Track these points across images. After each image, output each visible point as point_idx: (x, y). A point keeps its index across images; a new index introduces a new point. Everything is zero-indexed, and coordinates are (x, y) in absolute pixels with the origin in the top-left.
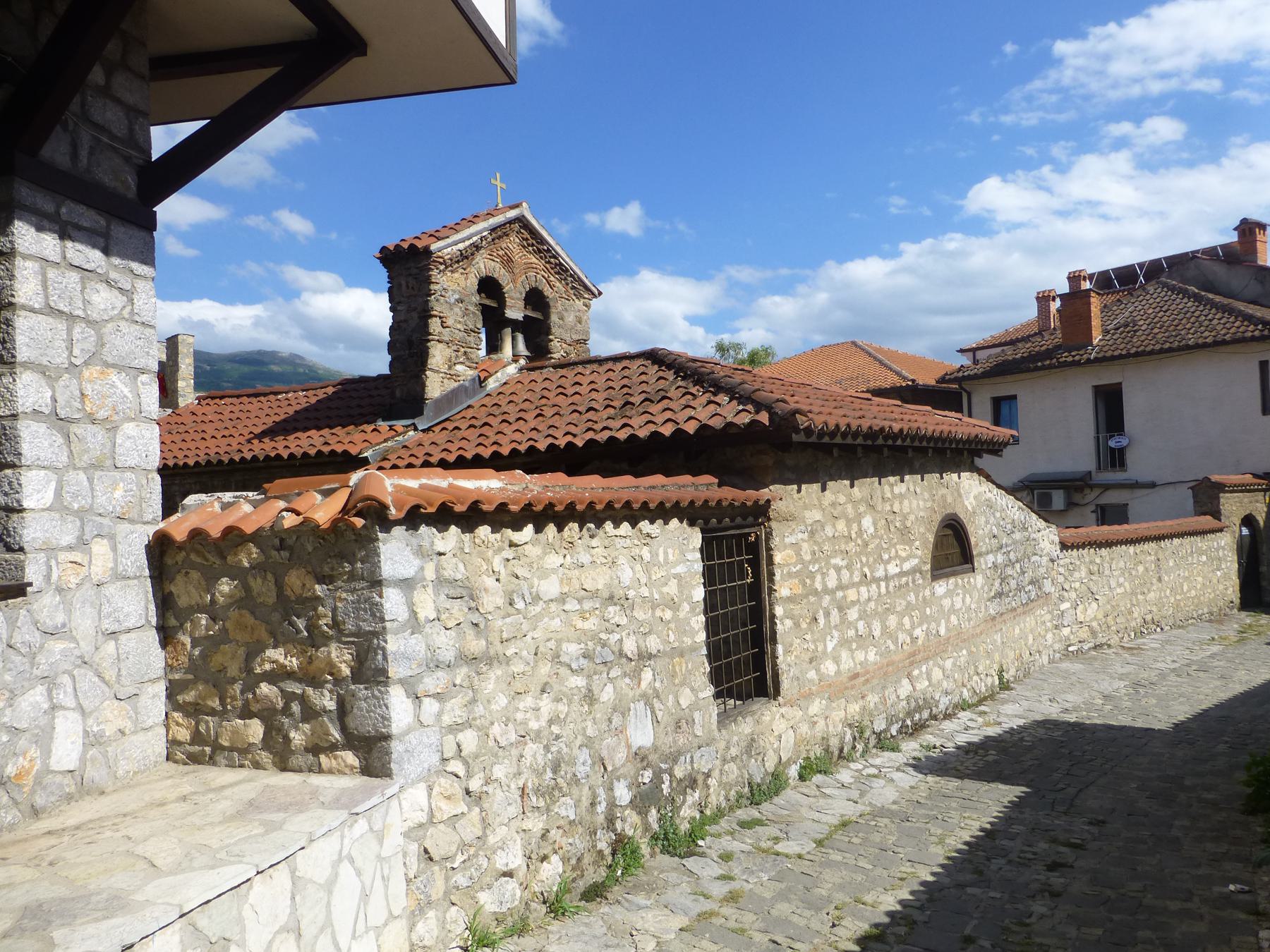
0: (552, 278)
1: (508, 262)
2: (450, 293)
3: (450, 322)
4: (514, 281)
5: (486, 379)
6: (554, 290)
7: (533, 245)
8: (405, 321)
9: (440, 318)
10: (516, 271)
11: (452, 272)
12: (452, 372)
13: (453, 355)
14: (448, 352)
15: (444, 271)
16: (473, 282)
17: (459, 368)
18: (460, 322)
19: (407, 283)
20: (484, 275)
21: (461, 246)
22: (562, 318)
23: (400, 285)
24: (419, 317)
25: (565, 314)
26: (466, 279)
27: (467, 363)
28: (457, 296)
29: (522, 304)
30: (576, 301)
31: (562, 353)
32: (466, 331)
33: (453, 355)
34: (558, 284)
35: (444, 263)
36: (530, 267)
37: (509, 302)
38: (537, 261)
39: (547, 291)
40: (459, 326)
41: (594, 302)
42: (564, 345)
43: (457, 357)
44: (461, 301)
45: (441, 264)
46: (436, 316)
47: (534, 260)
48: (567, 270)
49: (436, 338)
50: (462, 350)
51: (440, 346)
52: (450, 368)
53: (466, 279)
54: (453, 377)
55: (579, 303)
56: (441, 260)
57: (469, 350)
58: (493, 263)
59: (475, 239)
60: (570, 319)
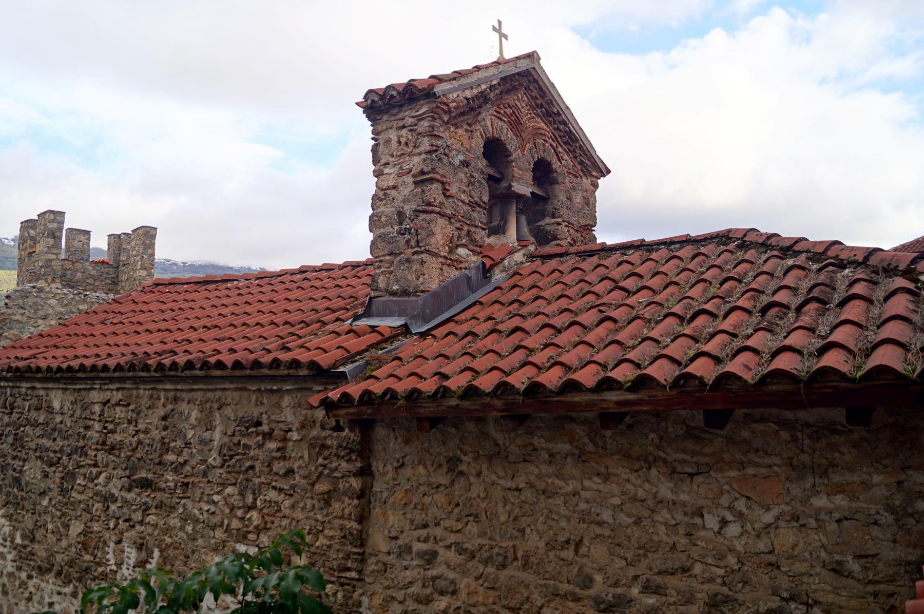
0: (560, 149)
1: (516, 124)
2: (454, 152)
3: (453, 190)
4: (522, 148)
5: (492, 267)
6: (562, 164)
7: (542, 106)
8: (394, 187)
9: (443, 183)
10: (524, 135)
11: (456, 126)
12: (453, 257)
13: (456, 233)
14: (450, 229)
15: (447, 123)
16: (478, 143)
17: (462, 251)
18: (464, 191)
19: (399, 137)
20: (490, 135)
21: (468, 94)
22: (569, 199)
23: (388, 141)
24: (416, 183)
25: (573, 194)
26: (470, 138)
27: (471, 247)
28: (461, 157)
29: (529, 176)
30: (584, 180)
31: (569, 240)
32: (470, 204)
33: (456, 233)
34: (566, 157)
35: (448, 112)
36: (537, 133)
37: (517, 172)
38: (545, 127)
39: (556, 165)
40: (463, 197)
41: (601, 181)
42: (572, 231)
43: (459, 237)
44: (465, 164)
45: (445, 112)
46: (438, 181)
47: (542, 125)
48: (577, 141)
49: (437, 209)
50: (466, 228)
51: (441, 221)
52: (451, 251)
53: (470, 138)
54: (455, 263)
55: (586, 182)
56: (445, 108)
57: (473, 229)
58: (500, 123)
59: (484, 87)
60: (578, 199)
